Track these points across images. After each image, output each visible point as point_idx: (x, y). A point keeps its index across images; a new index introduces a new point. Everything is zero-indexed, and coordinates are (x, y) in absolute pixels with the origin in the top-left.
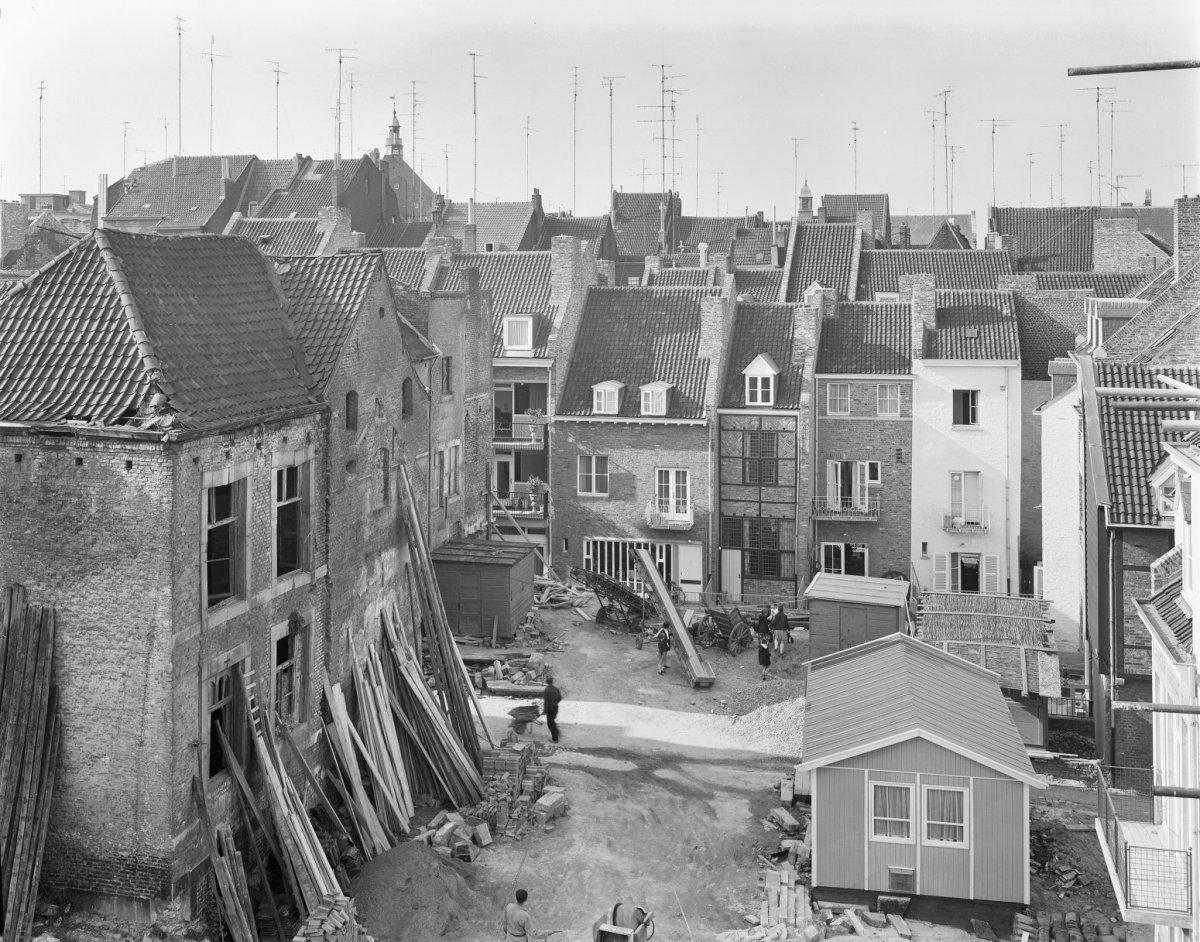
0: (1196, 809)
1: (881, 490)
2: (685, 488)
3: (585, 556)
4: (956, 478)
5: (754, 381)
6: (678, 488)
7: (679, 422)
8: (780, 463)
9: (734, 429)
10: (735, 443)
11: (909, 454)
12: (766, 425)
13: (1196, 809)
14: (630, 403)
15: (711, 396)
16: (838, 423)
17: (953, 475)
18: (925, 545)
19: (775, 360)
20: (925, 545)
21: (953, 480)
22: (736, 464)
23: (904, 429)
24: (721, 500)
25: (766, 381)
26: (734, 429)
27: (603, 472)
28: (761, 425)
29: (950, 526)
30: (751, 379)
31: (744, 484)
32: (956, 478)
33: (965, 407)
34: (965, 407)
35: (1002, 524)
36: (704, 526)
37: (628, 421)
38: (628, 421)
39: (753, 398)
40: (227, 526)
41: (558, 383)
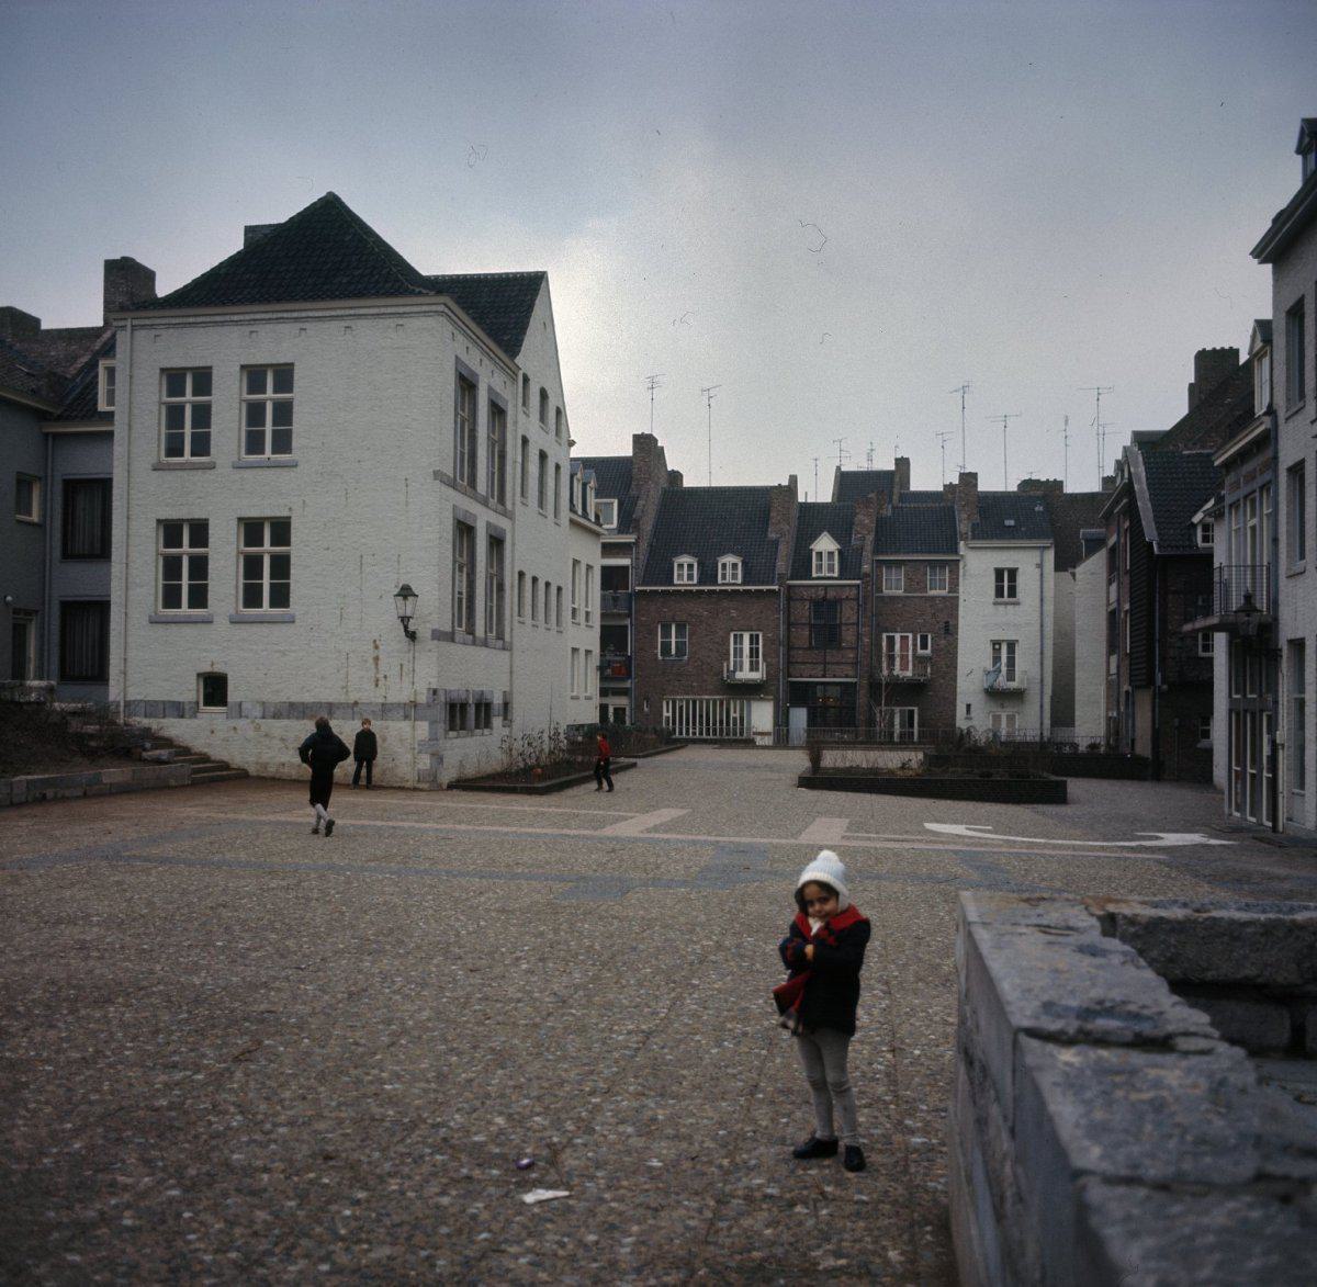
0: (986, 548)
1: (931, 658)
2: (757, 649)
3: (665, 714)
4: (997, 647)
5: (820, 554)
6: (751, 649)
7: (753, 588)
8: (844, 628)
9: (802, 599)
10: (803, 611)
11: (956, 627)
12: (831, 594)
13: (986, 548)
14: (708, 575)
15: (782, 565)
16: (893, 599)
17: (994, 644)
18: (969, 706)
19: (837, 538)
20: (969, 706)
21: (994, 649)
22: (803, 630)
23: (951, 604)
24: (789, 662)
25: (831, 554)
26: (802, 599)
27: (666, 638)
28: (826, 593)
29: (995, 694)
30: (817, 553)
31: (810, 648)
32: (997, 647)
33: (1006, 583)
34: (1006, 583)
35: (1038, 687)
36: (775, 682)
37: (706, 588)
38: (706, 588)
39: (820, 568)
40: (642, 585)
41: (642, 557)
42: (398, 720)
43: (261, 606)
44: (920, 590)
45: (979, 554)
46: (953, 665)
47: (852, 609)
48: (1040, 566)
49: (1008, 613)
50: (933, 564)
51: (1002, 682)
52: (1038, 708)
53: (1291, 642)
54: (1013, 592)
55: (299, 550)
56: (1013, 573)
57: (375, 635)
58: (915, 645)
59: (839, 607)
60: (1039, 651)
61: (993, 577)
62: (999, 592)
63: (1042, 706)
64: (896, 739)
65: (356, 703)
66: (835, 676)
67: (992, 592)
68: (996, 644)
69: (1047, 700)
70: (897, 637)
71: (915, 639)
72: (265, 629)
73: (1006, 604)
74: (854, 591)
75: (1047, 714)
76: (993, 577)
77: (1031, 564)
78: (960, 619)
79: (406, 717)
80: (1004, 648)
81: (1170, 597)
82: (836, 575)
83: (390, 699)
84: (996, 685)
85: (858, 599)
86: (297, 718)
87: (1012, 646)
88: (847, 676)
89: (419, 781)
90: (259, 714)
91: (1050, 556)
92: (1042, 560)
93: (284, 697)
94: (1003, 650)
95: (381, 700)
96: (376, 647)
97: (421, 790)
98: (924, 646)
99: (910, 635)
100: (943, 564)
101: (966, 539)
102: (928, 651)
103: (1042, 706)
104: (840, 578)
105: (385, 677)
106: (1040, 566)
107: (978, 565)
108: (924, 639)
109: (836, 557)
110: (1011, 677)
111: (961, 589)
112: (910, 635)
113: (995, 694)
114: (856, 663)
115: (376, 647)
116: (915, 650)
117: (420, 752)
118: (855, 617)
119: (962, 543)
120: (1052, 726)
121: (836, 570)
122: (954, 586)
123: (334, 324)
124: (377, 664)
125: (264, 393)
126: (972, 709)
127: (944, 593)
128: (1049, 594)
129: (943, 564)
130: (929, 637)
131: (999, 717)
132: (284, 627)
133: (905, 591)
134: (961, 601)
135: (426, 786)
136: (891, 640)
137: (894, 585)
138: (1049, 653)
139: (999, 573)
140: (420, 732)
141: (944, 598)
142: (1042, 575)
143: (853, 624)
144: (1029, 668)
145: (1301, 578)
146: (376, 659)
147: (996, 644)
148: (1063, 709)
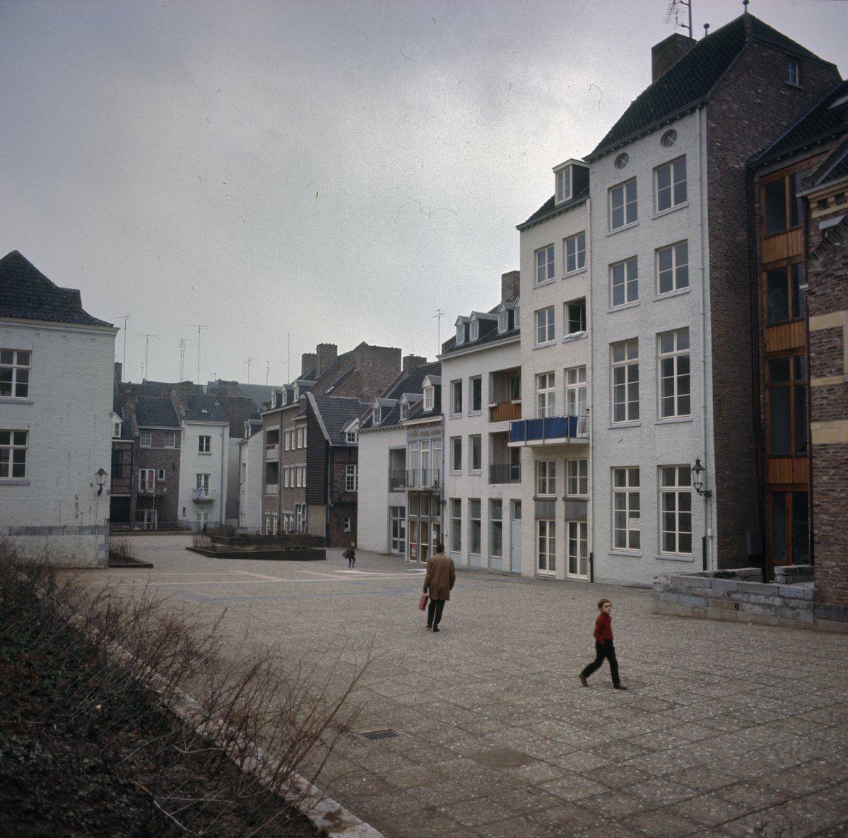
11: (179, 466)
16: (145, 450)
18: (184, 509)
20: (184, 509)
23: (176, 454)
29: (199, 503)
33: (204, 443)
34: (204, 443)
42: (88, 534)
43: (7, 476)
44: (160, 446)
45: (192, 427)
46: (177, 487)
47: (129, 456)
48: (222, 435)
49: (204, 460)
50: (167, 432)
51: (203, 496)
52: (219, 510)
53: (452, 499)
54: (208, 449)
55: (31, 445)
56: (208, 439)
57: (76, 492)
58: (156, 476)
59: (120, 455)
60: (220, 479)
61: (198, 441)
62: (201, 448)
63: (221, 509)
64: (156, 528)
65: (65, 527)
66: (118, 493)
67: (198, 448)
68: (199, 476)
69: (224, 505)
70: (147, 471)
71: (156, 472)
72: (11, 489)
73: (204, 455)
74: (129, 447)
75: (224, 513)
76: (198, 441)
77: (218, 435)
78: (181, 462)
79: (92, 533)
80: (203, 478)
81: (335, 465)
82: (120, 436)
83: (84, 524)
84: (200, 498)
85: (132, 451)
86: (31, 535)
87: (207, 477)
88: (125, 493)
89: (99, 564)
90: (8, 533)
91: (227, 431)
92: (223, 433)
93: (22, 524)
94: (203, 480)
95: (79, 525)
96: (77, 498)
97: (100, 569)
98: (161, 476)
99: (154, 470)
100: (172, 432)
101: (185, 419)
102: (164, 479)
103: (221, 509)
104: (122, 438)
105: (82, 513)
106: (222, 435)
107: (191, 434)
108: (161, 472)
109: (120, 426)
110: (207, 494)
111: (182, 446)
112: (154, 470)
113: (199, 503)
114: (131, 486)
115: (77, 498)
116: (156, 478)
117: (100, 550)
118: (130, 460)
119: (183, 421)
120: (226, 518)
121: (120, 434)
122: (178, 444)
123: (57, 334)
124: (77, 507)
125: (12, 363)
126: (186, 510)
127: (173, 448)
128: (226, 450)
129: (172, 432)
130: (164, 471)
131: (200, 514)
132: (25, 488)
133: (152, 446)
134: (182, 452)
135: (103, 567)
136: (143, 473)
137: (147, 444)
138: (225, 481)
139: (201, 438)
140: (100, 540)
141: (173, 450)
142: (223, 440)
143: (128, 464)
144: (216, 489)
145: (459, 477)
146: (77, 504)
147: (199, 476)
148: (233, 508)
